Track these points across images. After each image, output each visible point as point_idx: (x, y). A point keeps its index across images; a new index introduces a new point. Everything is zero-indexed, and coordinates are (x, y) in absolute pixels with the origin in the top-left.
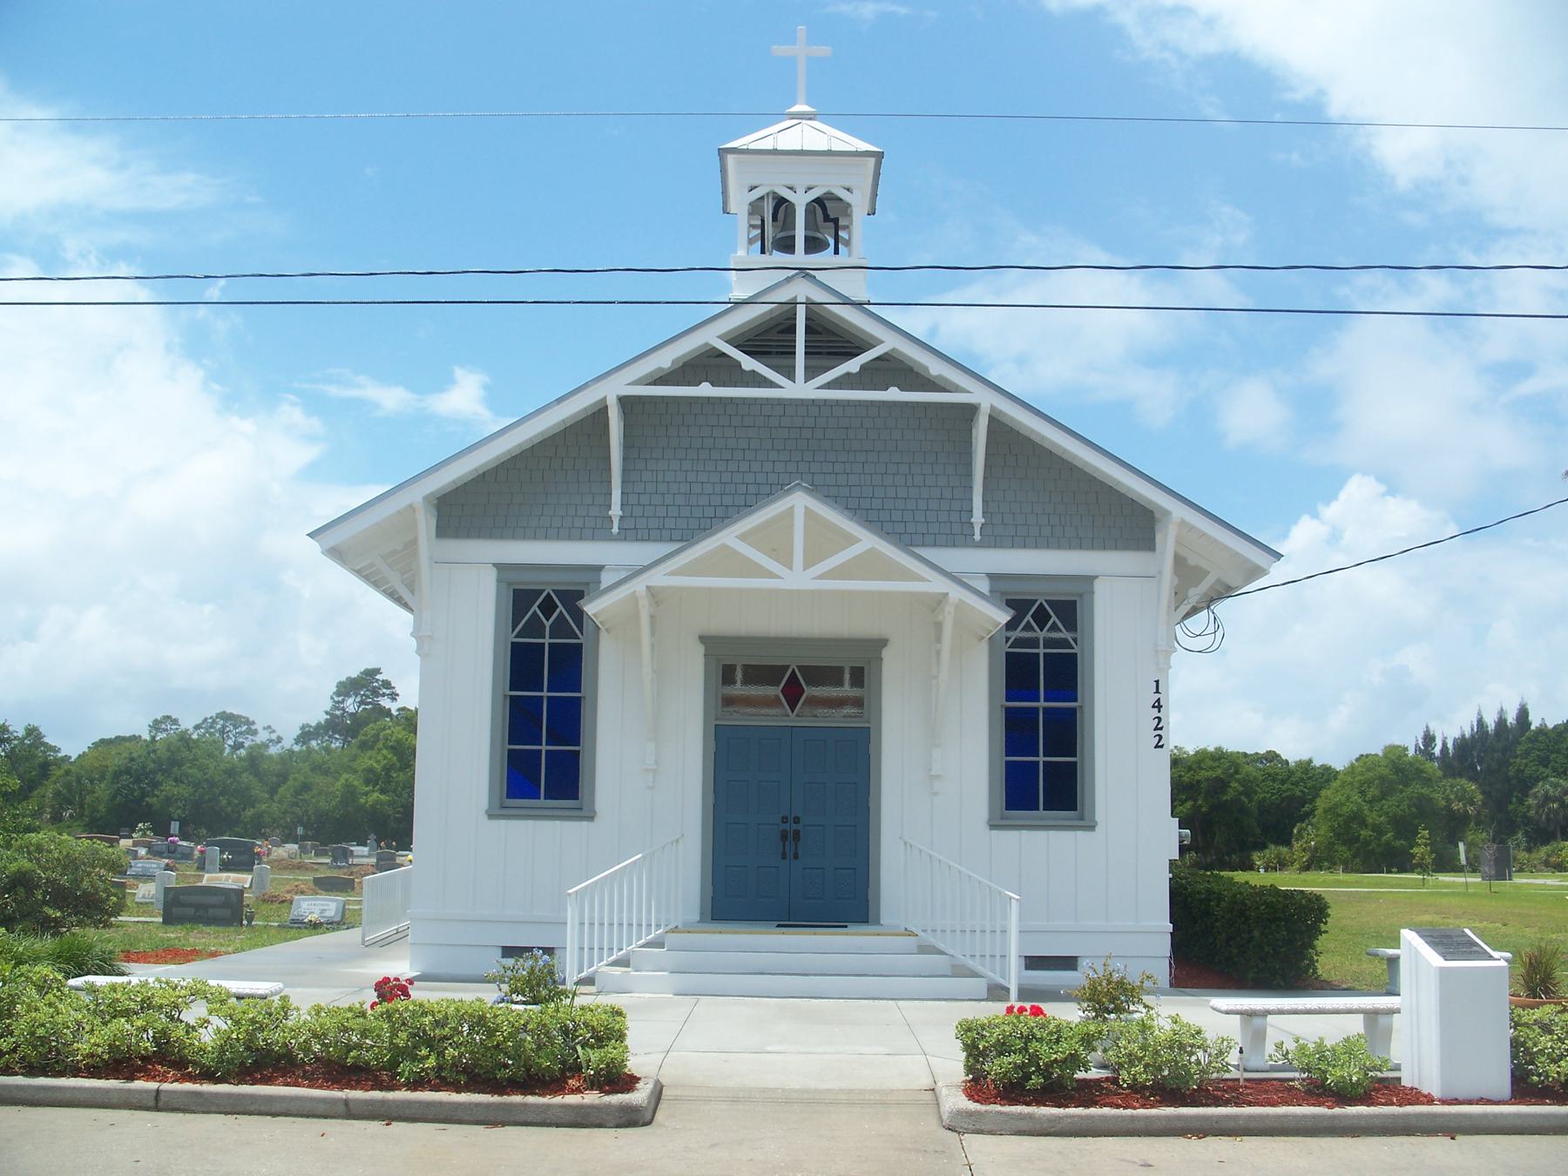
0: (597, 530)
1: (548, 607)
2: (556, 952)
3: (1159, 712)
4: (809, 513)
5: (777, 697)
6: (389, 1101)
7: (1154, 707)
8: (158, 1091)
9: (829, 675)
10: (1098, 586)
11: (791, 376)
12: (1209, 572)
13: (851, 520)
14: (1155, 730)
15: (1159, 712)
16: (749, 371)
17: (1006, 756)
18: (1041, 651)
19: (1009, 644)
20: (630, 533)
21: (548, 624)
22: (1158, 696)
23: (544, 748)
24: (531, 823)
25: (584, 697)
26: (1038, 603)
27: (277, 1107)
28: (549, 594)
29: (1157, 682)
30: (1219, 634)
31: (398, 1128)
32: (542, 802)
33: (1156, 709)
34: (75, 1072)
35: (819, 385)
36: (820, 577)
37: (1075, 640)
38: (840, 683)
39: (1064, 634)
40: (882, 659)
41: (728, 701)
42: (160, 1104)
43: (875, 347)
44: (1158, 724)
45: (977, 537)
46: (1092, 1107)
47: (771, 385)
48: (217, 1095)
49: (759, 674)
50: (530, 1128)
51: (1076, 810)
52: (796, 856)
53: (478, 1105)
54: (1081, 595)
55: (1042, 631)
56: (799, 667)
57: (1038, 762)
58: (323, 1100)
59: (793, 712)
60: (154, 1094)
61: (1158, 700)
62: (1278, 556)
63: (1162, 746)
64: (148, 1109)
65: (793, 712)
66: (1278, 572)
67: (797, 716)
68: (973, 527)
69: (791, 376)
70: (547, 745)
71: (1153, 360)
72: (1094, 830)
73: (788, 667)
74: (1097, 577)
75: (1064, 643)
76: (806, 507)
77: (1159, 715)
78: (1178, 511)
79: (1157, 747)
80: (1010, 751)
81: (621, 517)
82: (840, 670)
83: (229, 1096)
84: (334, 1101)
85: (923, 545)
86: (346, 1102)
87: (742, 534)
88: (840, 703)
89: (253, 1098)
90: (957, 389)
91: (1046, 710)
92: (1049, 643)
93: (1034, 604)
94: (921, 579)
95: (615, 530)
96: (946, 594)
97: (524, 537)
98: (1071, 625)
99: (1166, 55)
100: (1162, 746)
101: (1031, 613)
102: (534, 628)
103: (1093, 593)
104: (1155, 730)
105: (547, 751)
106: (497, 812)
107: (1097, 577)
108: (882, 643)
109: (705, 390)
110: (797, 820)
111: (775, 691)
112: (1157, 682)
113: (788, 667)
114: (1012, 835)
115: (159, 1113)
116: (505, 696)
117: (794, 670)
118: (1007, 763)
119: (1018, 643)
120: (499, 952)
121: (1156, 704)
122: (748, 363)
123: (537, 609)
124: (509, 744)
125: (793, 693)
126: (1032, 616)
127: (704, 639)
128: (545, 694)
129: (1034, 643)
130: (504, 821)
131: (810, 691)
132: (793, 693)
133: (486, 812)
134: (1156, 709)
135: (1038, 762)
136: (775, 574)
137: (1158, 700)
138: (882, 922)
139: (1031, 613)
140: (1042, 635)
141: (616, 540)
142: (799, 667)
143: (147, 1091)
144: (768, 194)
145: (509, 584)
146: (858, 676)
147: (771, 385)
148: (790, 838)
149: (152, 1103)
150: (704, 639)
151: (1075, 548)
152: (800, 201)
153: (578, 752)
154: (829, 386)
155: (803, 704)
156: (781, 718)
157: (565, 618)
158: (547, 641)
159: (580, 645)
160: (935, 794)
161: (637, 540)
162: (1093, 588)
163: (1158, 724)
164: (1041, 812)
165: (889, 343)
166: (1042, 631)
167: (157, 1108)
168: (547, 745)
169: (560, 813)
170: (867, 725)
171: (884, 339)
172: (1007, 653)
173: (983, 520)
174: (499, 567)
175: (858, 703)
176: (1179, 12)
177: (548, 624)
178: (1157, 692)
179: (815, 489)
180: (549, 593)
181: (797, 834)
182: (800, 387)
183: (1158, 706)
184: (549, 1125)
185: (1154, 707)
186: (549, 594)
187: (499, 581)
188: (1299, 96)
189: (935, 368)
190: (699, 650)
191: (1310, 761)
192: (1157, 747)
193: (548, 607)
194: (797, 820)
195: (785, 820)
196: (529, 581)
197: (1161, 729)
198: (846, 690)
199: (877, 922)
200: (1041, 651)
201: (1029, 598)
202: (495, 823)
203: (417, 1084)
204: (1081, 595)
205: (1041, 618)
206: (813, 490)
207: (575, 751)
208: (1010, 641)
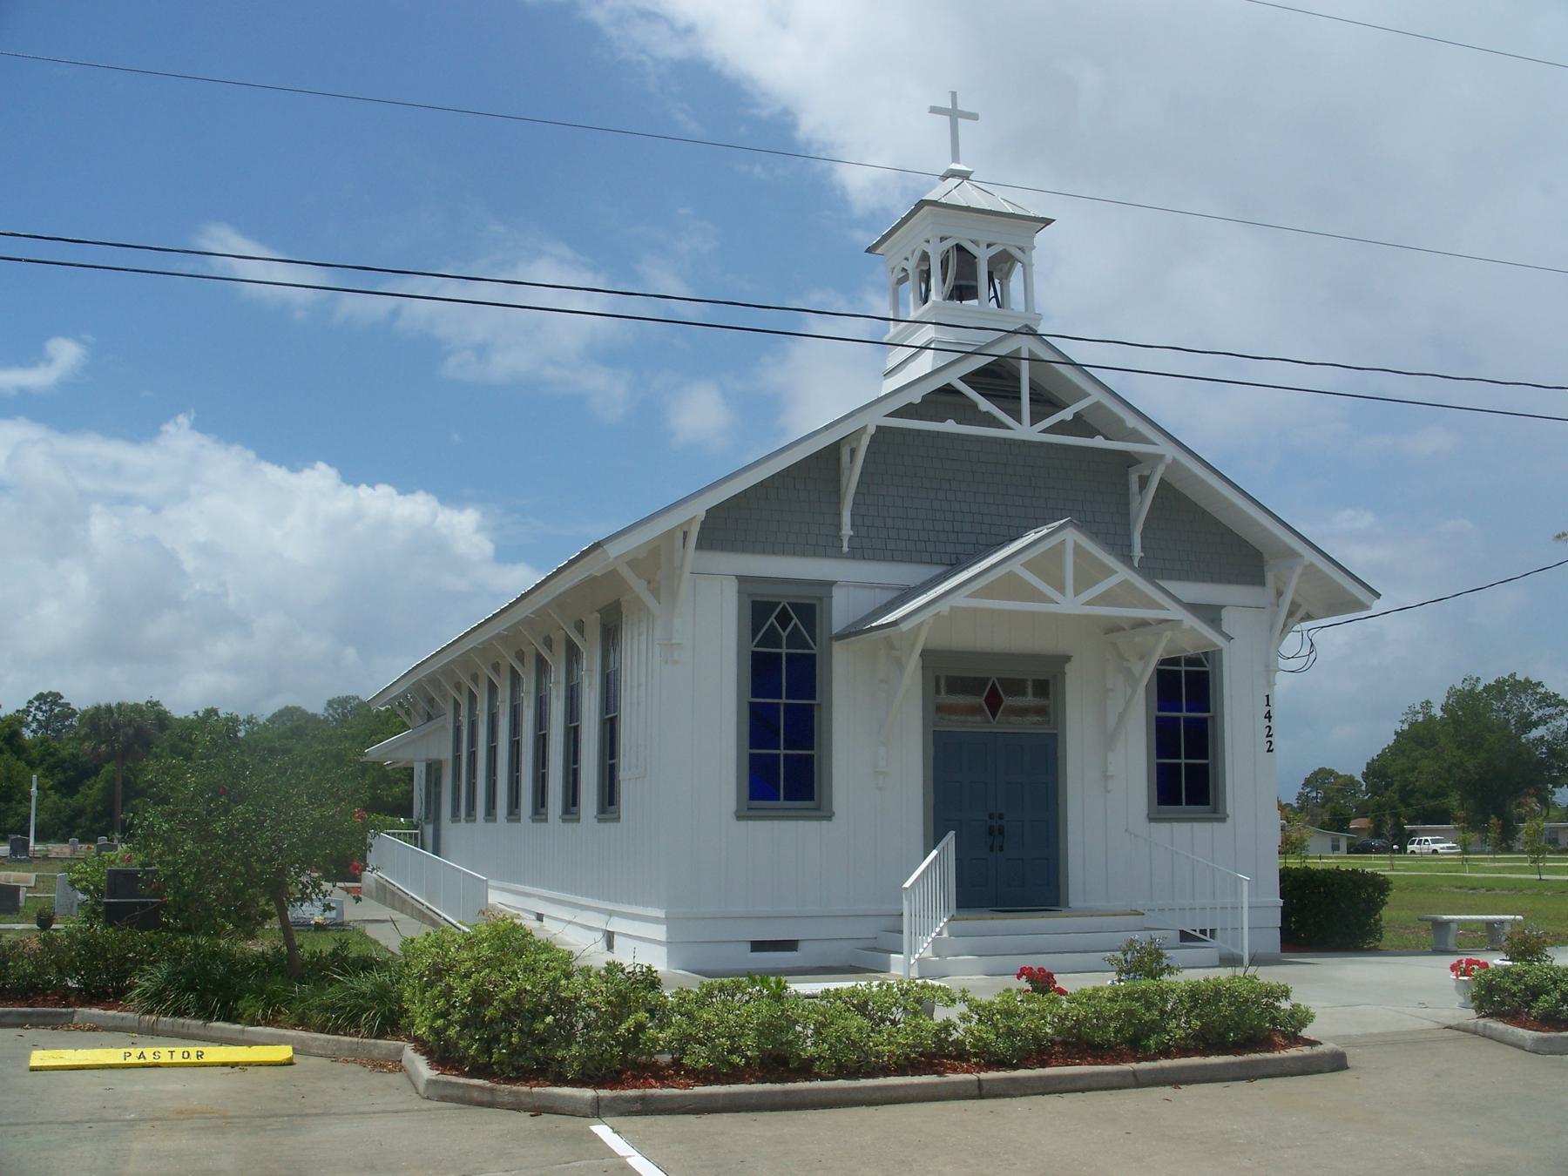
0: (828, 547)
1: (784, 619)
2: (800, 945)
3: (1270, 721)
4: (1077, 547)
5: (981, 706)
6: (1167, 1069)
7: (1266, 717)
9: (1016, 687)
11: (1017, 416)
13: (1110, 554)
15: (1270, 721)
16: (985, 412)
17: (751, 748)
18: (1183, 668)
20: (859, 552)
21: (784, 635)
23: (782, 752)
24: (767, 824)
25: (819, 705)
26: (781, 606)
27: (1080, 1085)
28: (784, 607)
29: (1268, 696)
30: (1313, 656)
31: (1185, 1090)
32: (782, 803)
33: (1267, 720)
34: (886, 1071)
36: (1088, 603)
38: (1024, 694)
40: (1065, 673)
41: (940, 709)
42: (984, 1092)
44: (1269, 732)
45: (845, 548)
46: (1211, 1055)
48: (1029, 1079)
49: (957, 685)
51: (1208, 804)
52: (1001, 849)
53: (1234, 1064)
54: (820, 599)
56: (998, 679)
57: (779, 755)
58: (1117, 1074)
59: (994, 719)
60: (977, 1084)
61: (1269, 712)
62: (1378, 595)
63: (1272, 751)
64: (973, 1098)
65: (994, 719)
66: (1377, 606)
68: (841, 540)
69: (1017, 416)
70: (784, 749)
71: (606, 356)
74: (1224, 606)
76: (1075, 541)
78: (1309, 556)
79: (1269, 751)
80: (754, 744)
81: (851, 536)
82: (1023, 681)
83: (1040, 1078)
84: (1124, 1074)
85: (1162, 578)
86: (1134, 1073)
87: (1025, 563)
88: (1024, 711)
89: (1059, 1078)
91: (1186, 719)
93: (777, 607)
94: (1162, 608)
96: (1181, 621)
97: (764, 552)
99: (644, 58)
100: (1272, 751)
102: (771, 638)
105: (785, 755)
107: (1224, 606)
108: (1067, 659)
109: (950, 426)
110: (1001, 817)
112: (1268, 696)
113: (988, 679)
114: (1165, 827)
115: (983, 1101)
118: (751, 755)
120: (749, 946)
122: (985, 405)
123: (775, 621)
125: (994, 702)
126: (775, 618)
131: (1008, 701)
132: (994, 702)
134: (1267, 720)
135: (779, 755)
136: (1049, 597)
137: (1269, 712)
138: (1070, 905)
141: (847, 558)
142: (998, 679)
143: (971, 1082)
144: (953, 247)
145: (750, 595)
146: (1042, 688)
149: (976, 1092)
151: (788, 554)
152: (983, 256)
155: (1002, 712)
156: (976, 725)
157: (800, 630)
158: (784, 651)
159: (814, 655)
160: (1109, 792)
161: (864, 559)
162: (1220, 615)
163: (1269, 732)
164: (1184, 807)
167: (981, 1096)
168: (784, 749)
169: (781, 813)
170: (1055, 732)
171: (1091, 393)
172: (753, 652)
173: (852, 533)
174: (741, 579)
175: (1041, 711)
176: (650, 16)
177: (784, 635)
178: (1268, 705)
179: (1083, 525)
181: (1001, 832)
182: (1025, 430)
183: (1268, 716)
184: (1285, 1075)
185: (1266, 717)
187: (739, 592)
188: (765, 113)
189: (1131, 422)
192: (1269, 751)
193: (784, 619)
194: (1001, 817)
195: (991, 816)
198: (1030, 700)
199: (1067, 905)
200: (1183, 668)
201: (770, 599)
202: (743, 824)
203: (1166, 1053)
204: (820, 599)
206: (1082, 527)
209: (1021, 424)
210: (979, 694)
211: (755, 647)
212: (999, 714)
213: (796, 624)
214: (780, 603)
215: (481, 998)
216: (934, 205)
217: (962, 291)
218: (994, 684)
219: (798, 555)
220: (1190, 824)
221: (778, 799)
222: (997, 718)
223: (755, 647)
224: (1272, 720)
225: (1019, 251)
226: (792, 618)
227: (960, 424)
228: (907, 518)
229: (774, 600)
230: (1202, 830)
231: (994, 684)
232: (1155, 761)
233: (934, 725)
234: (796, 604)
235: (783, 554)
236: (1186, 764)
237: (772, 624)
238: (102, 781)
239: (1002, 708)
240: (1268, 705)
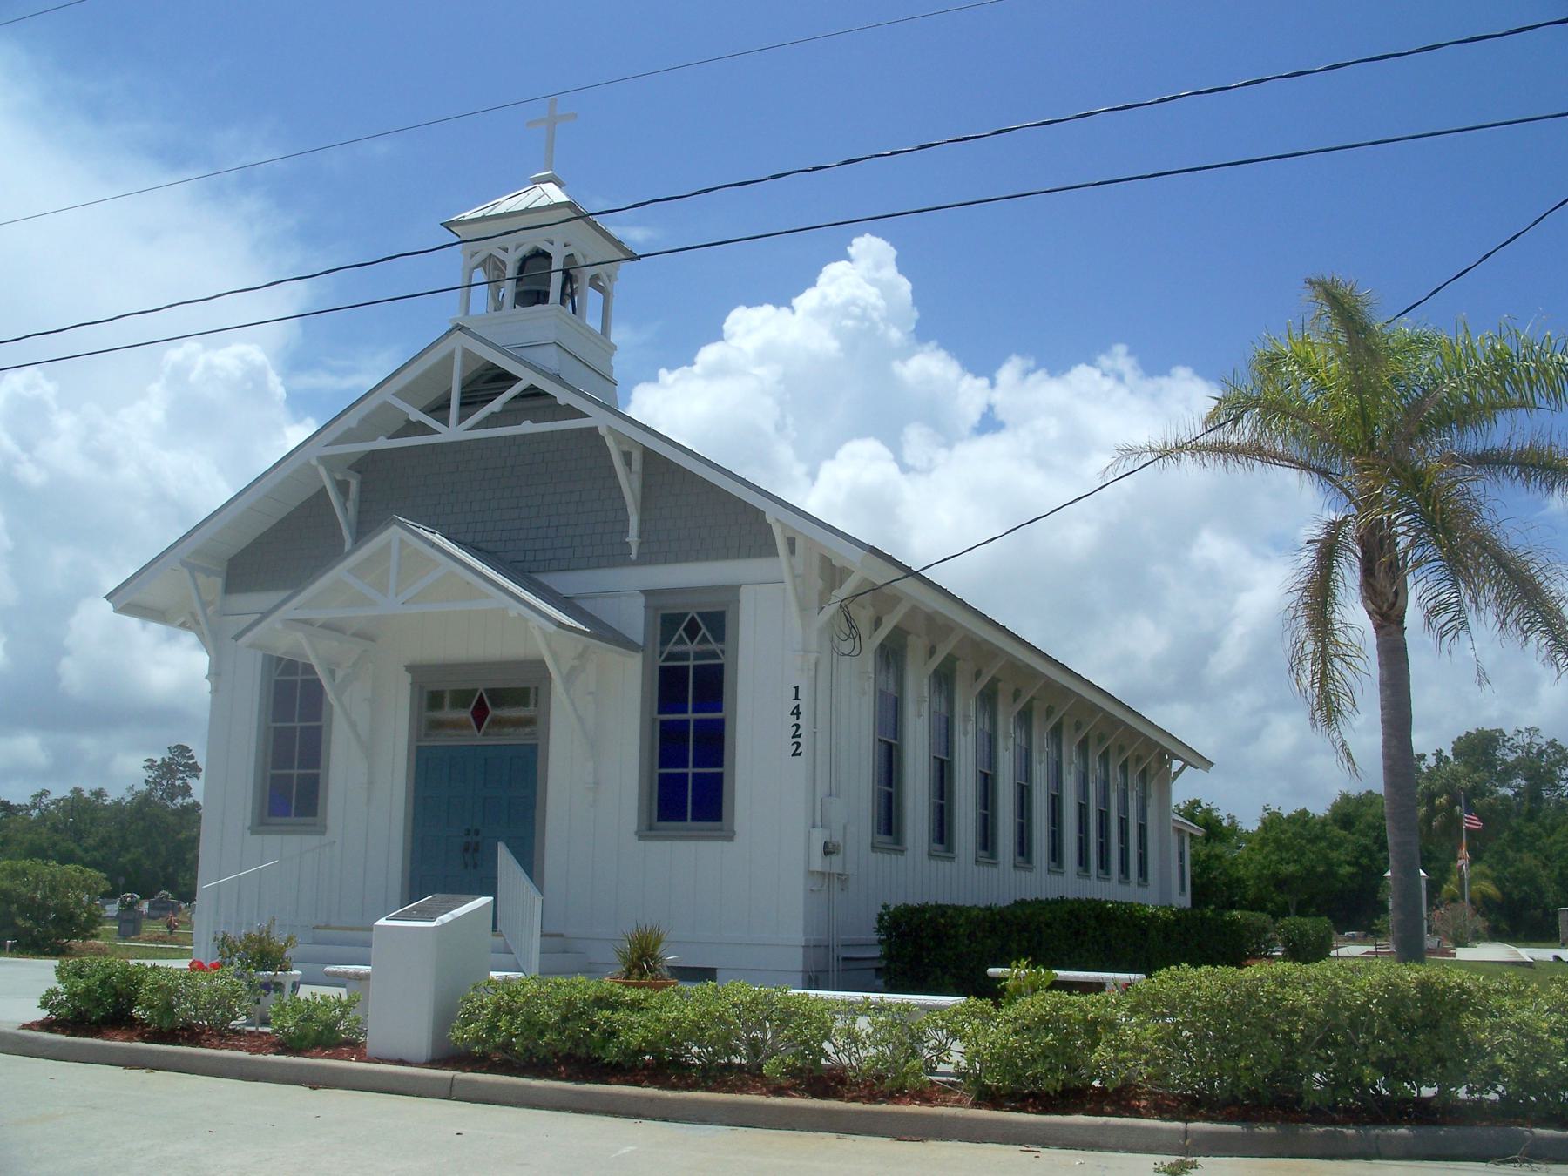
1: (692, 630)
3: (798, 718)
7: (792, 714)
8: (1186, 1132)
10: (746, 596)
12: (853, 572)
14: (793, 737)
15: (798, 718)
18: (691, 663)
19: (662, 658)
22: (797, 702)
23: (690, 770)
28: (693, 617)
29: (797, 688)
32: (293, 819)
35: (466, 427)
37: (723, 652)
39: (713, 646)
43: (451, 388)
47: (434, 432)
49: (461, 698)
50: (933, 1146)
55: (692, 643)
56: (698, 614)
67: (484, 735)
70: (298, 768)
72: (733, 841)
73: (477, 690)
74: (741, 586)
75: (714, 655)
77: (797, 722)
90: (584, 416)
92: (698, 656)
93: (685, 618)
95: (634, 556)
98: (719, 636)
100: (800, 754)
101: (682, 628)
103: (739, 601)
104: (793, 737)
105: (695, 766)
106: (646, 832)
109: (527, 427)
110: (477, 832)
111: (466, 715)
112: (797, 688)
113: (477, 690)
116: (654, 720)
117: (481, 694)
119: (671, 657)
121: (795, 711)
124: (273, 768)
127: (410, 668)
128: (297, 724)
129: (685, 656)
130: (720, 842)
131: (493, 713)
132: (480, 713)
133: (636, 833)
134: (795, 716)
139: (682, 628)
140: (691, 647)
142: (698, 614)
147: (434, 432)
148: (828, 850)
150: (410, 668)
153: (662, 765)
154: (478, 426)
155: (489, 724)
165: (528, 378)
166: (692, 643)
170: (534, 742)
174: (648, 593)
178: (797, 698)
180: (693, 617)
183: (796, 712)
185: (792, 714)
186: (693, 617)
187: (646, 607)
190: (408, 678)
191: (99, 794)
194: (477, 832)
195: (468, 832)
196: (675, 606)
197: (799, 736)
200: (691, 663)
205: (692, 630)
207: (718, 773)
208: (664, 655)
209: (609, 427)
210: (465, 706)
211: (663, 661)
212: (486, 724)
213: (704, 635)
214: (686, 614)
215: (1302, 1093)
216: (528, 213)
217: (533, 296)
218: (481, 697)
219: (670, 563)
220: (279, 837)
221: (685, 820)
222: (482, 730)
223: (663, 661)
224: (801, 716)
225: (520, 249)
226: (700, 629)
227: (537, 423)
228: (548, 527)
229: (682, 611)
230: (311, 841)
231: (481, 697)
232: (726, 770)
233: (418, 741)
234: (707, 613)
235: (665, 562)
236: (694, 774)
237: (681, 636)
238: (1500, 839)
239: (488, 719)
240: (797, 698)
